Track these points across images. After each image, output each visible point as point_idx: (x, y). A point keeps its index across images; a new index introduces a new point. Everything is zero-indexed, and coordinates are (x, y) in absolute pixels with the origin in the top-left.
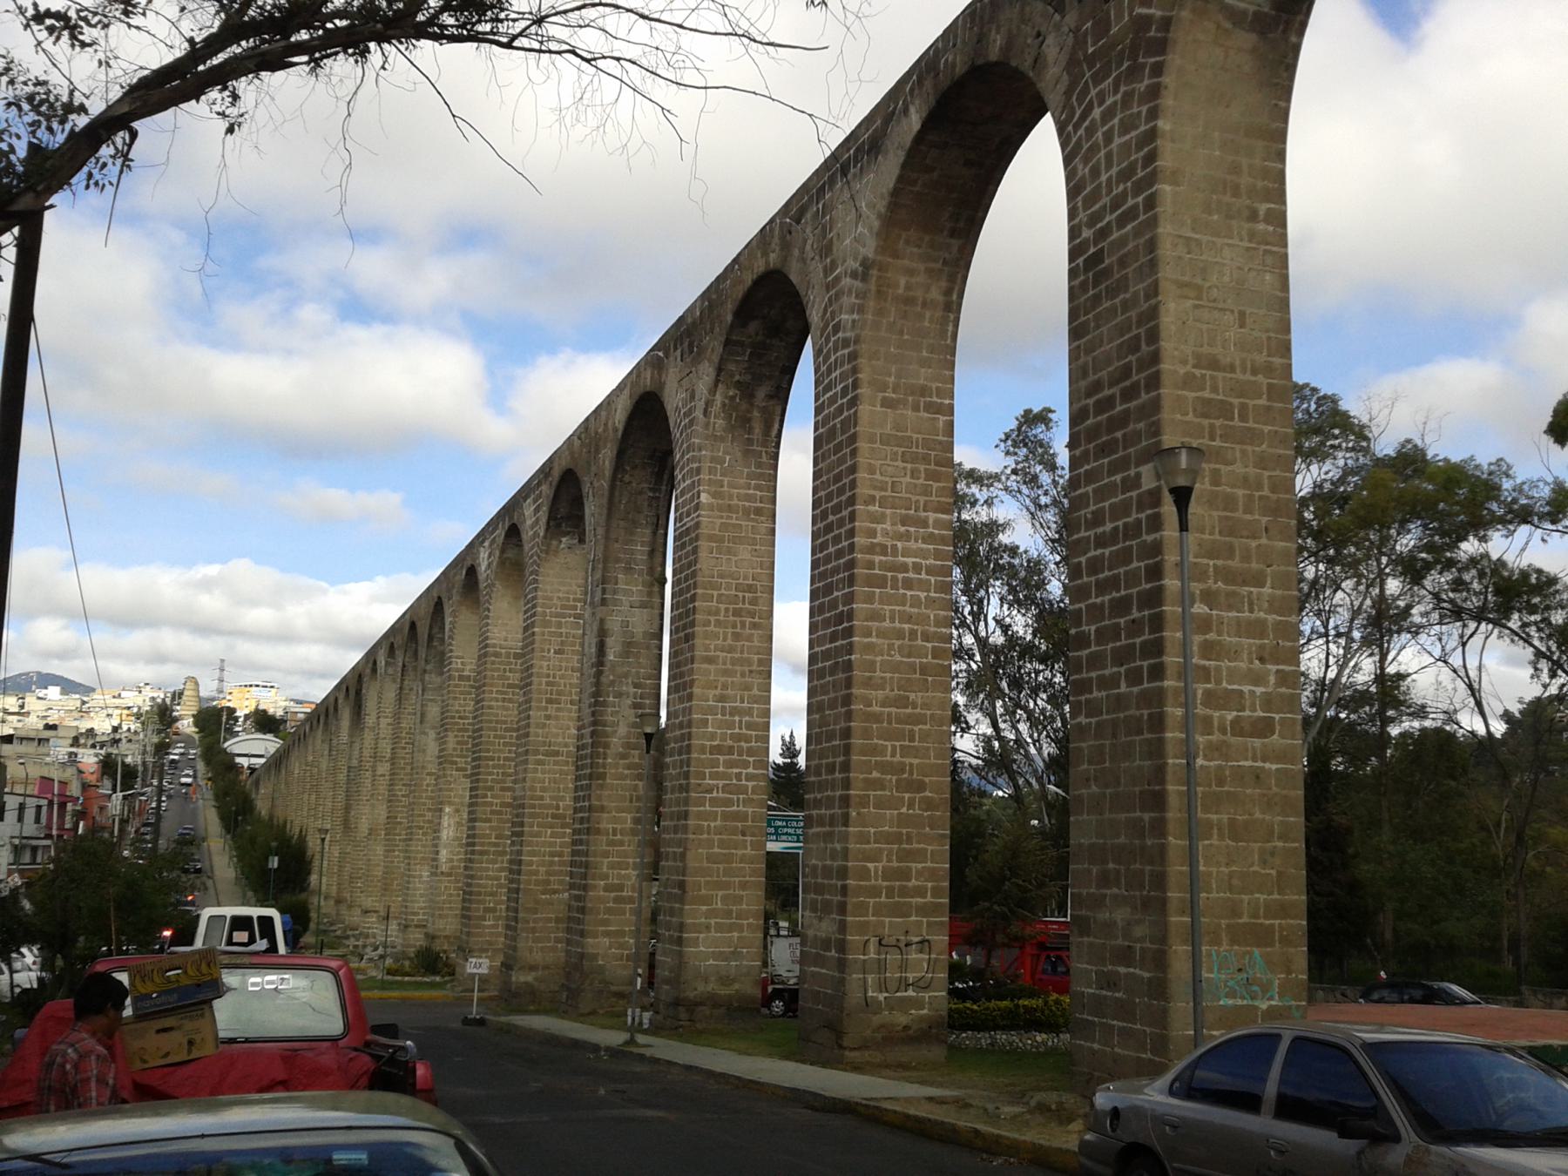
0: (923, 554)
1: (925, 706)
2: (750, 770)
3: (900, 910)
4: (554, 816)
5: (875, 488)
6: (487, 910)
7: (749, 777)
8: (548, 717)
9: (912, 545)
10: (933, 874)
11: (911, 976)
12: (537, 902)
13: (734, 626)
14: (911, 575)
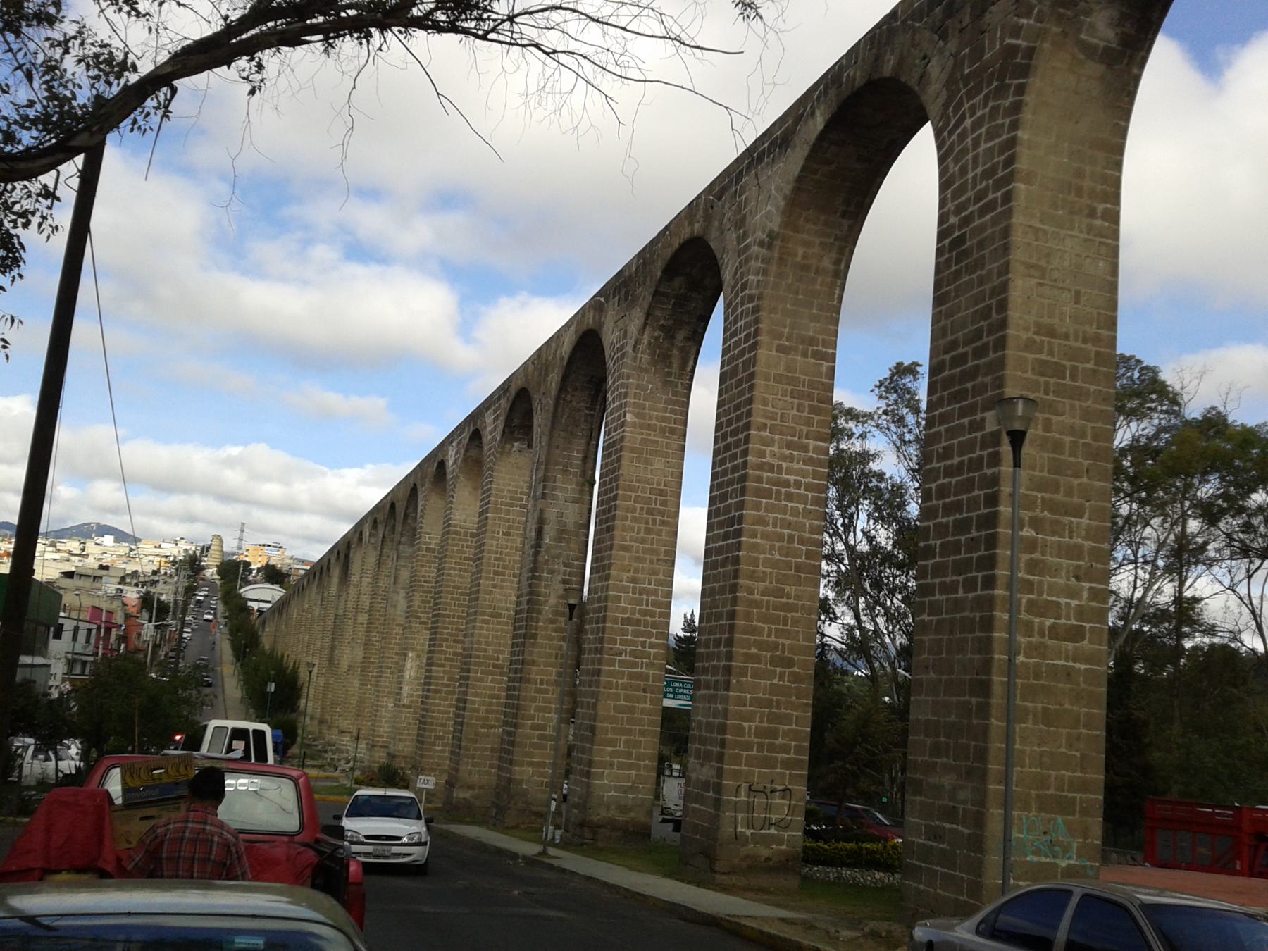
0: (803, 473)
1: (797, 597)
2: (653, 640)
3: (768, 763)
4: (495, 666)
5: (767, 417)
6: (438, 738)
7: (652, 646)
8: (494, 586)
9: (795, 465)
10: (795, 735)
11: (774, 817)
12: (477, 734)
13: (647, 523)
14: (792, 490)
